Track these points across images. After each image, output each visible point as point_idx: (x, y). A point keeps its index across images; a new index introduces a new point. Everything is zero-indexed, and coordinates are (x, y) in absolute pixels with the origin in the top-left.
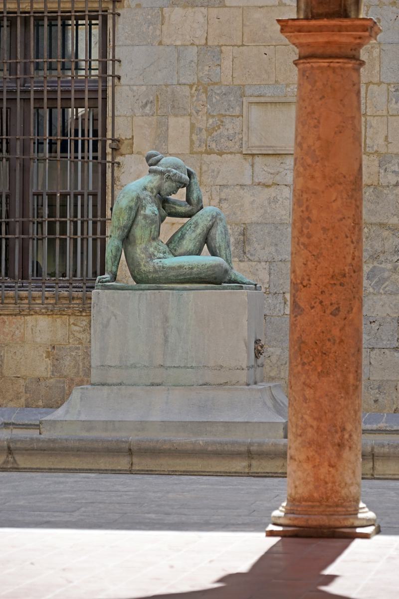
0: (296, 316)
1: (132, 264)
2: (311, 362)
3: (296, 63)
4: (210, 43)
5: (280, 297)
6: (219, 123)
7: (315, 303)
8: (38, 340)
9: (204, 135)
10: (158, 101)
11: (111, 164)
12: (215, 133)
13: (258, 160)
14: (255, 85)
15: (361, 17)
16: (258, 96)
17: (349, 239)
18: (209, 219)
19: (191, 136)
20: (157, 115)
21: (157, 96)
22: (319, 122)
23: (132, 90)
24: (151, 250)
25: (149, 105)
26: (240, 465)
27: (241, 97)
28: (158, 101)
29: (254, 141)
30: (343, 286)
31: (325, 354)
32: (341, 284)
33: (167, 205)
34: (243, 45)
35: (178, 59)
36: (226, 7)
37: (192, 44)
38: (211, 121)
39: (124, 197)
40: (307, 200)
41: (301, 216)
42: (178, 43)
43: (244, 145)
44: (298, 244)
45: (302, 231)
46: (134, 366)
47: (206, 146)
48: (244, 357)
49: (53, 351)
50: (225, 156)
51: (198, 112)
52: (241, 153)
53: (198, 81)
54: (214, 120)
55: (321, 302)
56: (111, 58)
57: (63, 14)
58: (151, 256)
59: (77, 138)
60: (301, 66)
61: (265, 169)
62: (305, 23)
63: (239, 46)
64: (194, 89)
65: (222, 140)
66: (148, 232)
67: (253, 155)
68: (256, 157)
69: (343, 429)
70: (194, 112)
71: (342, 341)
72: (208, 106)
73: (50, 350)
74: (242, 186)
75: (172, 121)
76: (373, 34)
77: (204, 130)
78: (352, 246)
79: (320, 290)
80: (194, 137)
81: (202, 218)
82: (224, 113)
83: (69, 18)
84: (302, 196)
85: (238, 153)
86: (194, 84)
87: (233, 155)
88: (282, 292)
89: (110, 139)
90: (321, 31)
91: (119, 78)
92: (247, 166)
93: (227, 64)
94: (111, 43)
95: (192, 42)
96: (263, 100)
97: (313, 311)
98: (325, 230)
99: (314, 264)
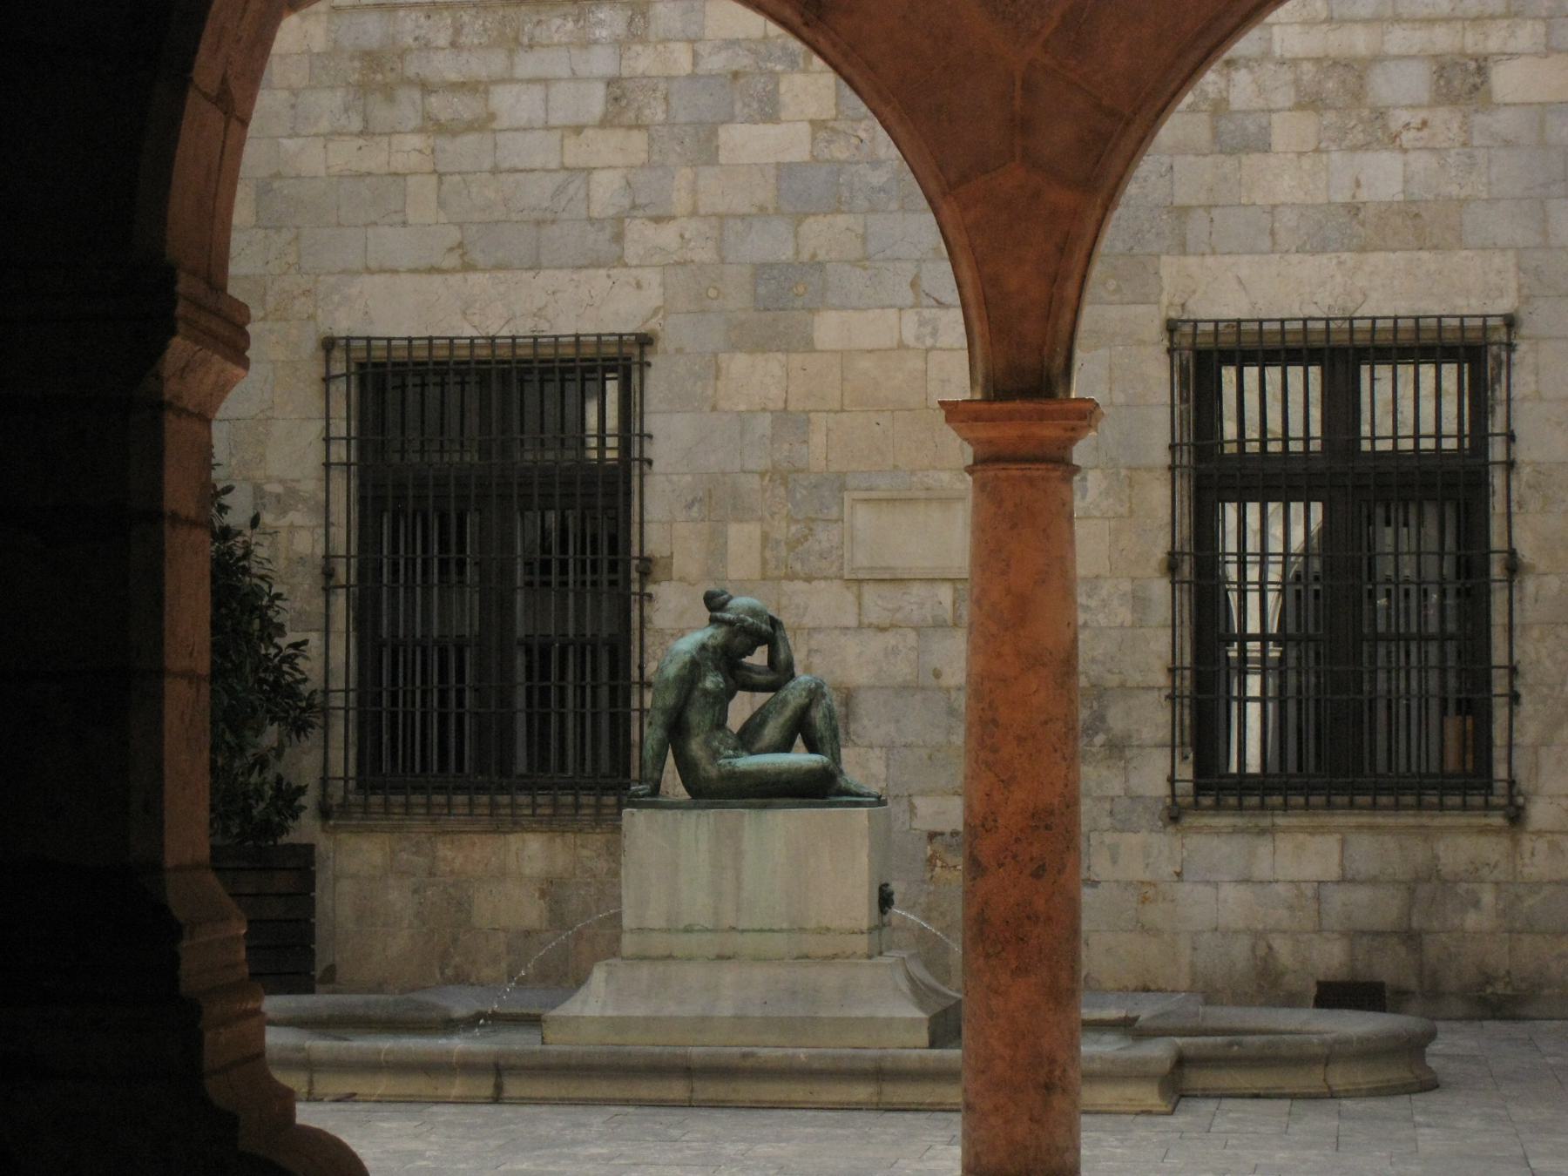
0: (974, 878)
1: (687, 768)
2: (999, 953)
3: (970, 470)
4: (791, 408)
5: (905, 801)
6: (807, 531)
7: (1005, 858)
8: (527, 871)
9: (783, 551)
10: (710, 497)
11: (638, 597)
12: (800, 548)
13: (868, 590)
14: (862, 472)
15: (1073, 396)
16: (867, 490)
17: (1059, 755)
18: (804, 694)
19: (762, 553)
20: (709, 520)
21: (710, 490)
22: (1008, 565)
23: (670, 481)
24: (716, 744)
25: (697, 505)
26: (862, 1092)
27: (840, 491)
28: (710, 497)
29: (862, 559)
30: (1051, 830)
31: (1022, 939)
32: (1048, 827)
33: (737, 672)
34: (843, 411)
35: (742, 434)
36: (816, 351)
37: (764, 410)
38: (793, 529)
39: (671, 661)
40: (991, 692)
41: (980, 717)
42: (742, 407)
43: (845, 566)
44: (976, 762)
45: (983, 739)
46: (688, 930)
47: (786, 567)
48: (862, 910)
49: (552, 889)
50: (815, 583)
51: (773, 515)
52: (841, 578)
53: (774, 467)
54: (799, 526)
55: (1014, 857)
56: (637, 431)
57: (563, 365)
58: (715, 755)
59: (584, 557)
60: (978, 475)
61: (880, 603)
62: (984, 406)
63: (837, 412)
64: (767, 478)
65: (811, 558)
66: (709, 716)
67: (860, 581)
68: (865, 584)
69: (1053, 1061)
70: (768, 516)
71: (1049, 919)
72: (790, 506)
73: (545, 886)
74: (845, 629)
75: (734, 530)
76: (1093, 423)
77: (783, 543)
78: (1064, 764)
79: (1014, 837)
80: (768, 554)
81: (794, 694)
82: (814, 516)
83: (572, 370)
84: (982, 684)
85: (836, 578)
86: (767, 471)
87: (829, 581)
88: (906, 794)
89: (637, 558)
90: (1011, 419)
91: (650, 462)
92: (850, 597)
93: (818, 439)
94: (638, 409)
95: (763, 406)
96: (874, 495)
97: (1001, 870)
98: (1020, 740)
99: (1003, 794)
